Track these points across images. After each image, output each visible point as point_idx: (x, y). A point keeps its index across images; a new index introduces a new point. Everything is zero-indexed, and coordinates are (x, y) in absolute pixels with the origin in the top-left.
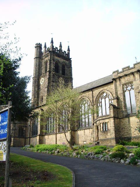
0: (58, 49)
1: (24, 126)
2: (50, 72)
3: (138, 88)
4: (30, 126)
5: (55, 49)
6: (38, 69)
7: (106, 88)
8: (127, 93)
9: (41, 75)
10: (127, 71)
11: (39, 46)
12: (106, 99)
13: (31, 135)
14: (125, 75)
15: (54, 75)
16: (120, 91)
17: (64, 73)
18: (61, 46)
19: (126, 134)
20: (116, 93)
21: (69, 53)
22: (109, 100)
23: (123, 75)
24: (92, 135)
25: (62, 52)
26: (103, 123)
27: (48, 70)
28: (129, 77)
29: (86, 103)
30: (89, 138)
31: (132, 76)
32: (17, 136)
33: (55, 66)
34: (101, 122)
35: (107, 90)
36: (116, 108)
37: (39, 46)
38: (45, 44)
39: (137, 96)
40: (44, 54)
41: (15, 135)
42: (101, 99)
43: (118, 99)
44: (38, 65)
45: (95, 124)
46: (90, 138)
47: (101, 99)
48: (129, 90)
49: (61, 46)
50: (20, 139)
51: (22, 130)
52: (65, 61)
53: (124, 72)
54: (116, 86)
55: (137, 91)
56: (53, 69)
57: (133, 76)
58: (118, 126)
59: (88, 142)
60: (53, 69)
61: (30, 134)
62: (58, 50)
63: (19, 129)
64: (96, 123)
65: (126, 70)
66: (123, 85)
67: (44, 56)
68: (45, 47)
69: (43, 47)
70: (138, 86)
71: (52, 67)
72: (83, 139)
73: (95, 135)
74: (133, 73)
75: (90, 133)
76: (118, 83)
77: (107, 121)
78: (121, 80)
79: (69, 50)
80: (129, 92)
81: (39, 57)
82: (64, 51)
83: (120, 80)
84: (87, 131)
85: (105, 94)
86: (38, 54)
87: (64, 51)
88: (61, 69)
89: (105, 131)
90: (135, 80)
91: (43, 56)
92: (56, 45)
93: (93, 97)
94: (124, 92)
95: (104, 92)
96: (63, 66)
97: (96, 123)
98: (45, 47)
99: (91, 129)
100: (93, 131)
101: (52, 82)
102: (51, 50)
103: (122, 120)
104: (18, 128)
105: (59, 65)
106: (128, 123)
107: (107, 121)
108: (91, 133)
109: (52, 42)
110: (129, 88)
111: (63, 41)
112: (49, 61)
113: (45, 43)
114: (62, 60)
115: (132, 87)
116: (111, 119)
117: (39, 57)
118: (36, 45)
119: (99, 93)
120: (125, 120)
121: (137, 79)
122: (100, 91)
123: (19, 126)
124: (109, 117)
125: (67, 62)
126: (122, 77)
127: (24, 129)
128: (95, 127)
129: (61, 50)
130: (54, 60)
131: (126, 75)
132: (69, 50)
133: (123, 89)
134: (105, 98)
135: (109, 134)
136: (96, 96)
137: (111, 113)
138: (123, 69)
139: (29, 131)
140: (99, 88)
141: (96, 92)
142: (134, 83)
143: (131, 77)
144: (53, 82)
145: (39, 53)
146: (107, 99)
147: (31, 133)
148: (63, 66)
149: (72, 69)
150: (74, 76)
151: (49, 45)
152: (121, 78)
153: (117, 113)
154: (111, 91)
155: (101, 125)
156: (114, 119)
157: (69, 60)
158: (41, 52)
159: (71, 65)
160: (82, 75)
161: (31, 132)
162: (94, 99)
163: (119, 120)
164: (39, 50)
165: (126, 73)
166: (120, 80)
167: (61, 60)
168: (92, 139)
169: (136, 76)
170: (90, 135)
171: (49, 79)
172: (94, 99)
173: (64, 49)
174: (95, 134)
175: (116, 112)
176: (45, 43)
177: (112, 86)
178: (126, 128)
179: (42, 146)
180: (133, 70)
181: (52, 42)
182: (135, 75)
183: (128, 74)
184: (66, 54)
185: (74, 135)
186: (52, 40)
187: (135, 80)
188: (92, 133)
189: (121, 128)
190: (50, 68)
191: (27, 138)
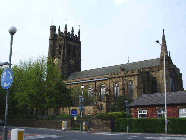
0: (71, 34)
2: (63, 55)
7: (104, 82)
8: (115, 88)
9: (55, 55)
11: (53, 29)
15: (66, 59)
16: (111, 86)
17: (74, 55)
18: (73, 31)
20: (109, 87)
21: (79, 36)
27: (62, 53)
29: (91, 89)
33: (68, 51)
34: (99, 103)
37: (53, 28)
38: (59, 28)
40: (58, 37)
42: (101, 88)
43: (110, 90)
44: (52, 46)
47: (101, 88)
49: (73, 31)
54: (109, 82)
56: (66, 53)
59: (91, 114)
60: (66, 53)
66: (113, 83)
68: (59, 30)
69: (57, 29)
71: (66, 51)
72: (88, 112)
73: (95, 110)
74: (119, 77)
76: (111, 81)
77: (102, 103)
79: (79, 33)
81: (53, 39)
84: (91, 108)
85: (103, 86)
86: (53, 36)
88: (72, 51)
89: (101, 108)
91: (57, 39)
92: (69, 30)
93: (96, 86)
94: (114, 87)
95: (102, 85)
96: (74, 49)
98: (59, 30)
101: (66, 64)
105: (71, 48)
107: (102, 103)
109: (66, 28)
110: (117, 85)
112: (63, 46)
113: (59, 26)
117: (53, 39)
125: (78, 45)
130: (67, 45)
131: (116, 77)
132: (79, 33)
133: (113, 85)
134: (103, 88)
135: (103, 111)
136: (98, 86)
141: (98, 84)
143: (118, 79)
144: (66, 64)
146: (104, 89)
148: (74, 49)
151: (63, 30)
155: (99, 105)
156: (106, 103)
160: (89, 62)
162: (97, 88)
166: (112, 80)
167: (73, 44)
171: (63, 61)
172: (97, 88)
176: (59, 26)
177: (108, 81)
179: (21, 129)
181: (66, 28)
184: (77, 38)
186: (66, 26)
188: (93, 109)
190: (64, 52)
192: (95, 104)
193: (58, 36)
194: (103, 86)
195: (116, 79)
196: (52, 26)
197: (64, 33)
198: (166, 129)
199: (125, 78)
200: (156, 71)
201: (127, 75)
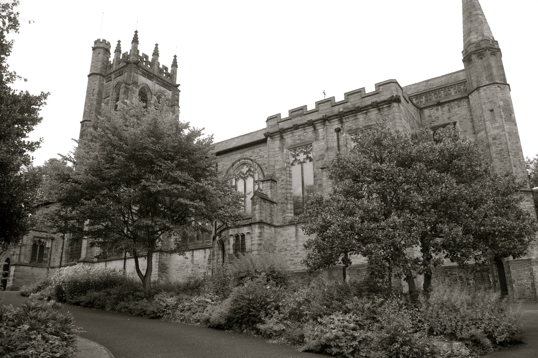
0: (150, 60)
1: (46, 239)
3: (323, 159)
4: (64, 239)
5: (141, 58)
6: (95, 103)
7: (248, 153)
10: (299, 118)
11: (101, 48)
12: (247, 181)
13: (63, 259)
14: (294, 125)
18: (156, 54)
19: (289, 262)
21: (174, 72)
22: (255, 182)
23: (291, 125)
24: (209, 263)
25: (159, 67)
26: (237, 236)
28: (303, 132)
30: (202, 271)
31: (310, 129)
32: (27, 262)
35: (252, 158)
36: (269, 201)
39: (318, 176)
41: (19, 259)
44: (96, 91)
45: (217, 238)
46: (206, 271)
48: (302, 160)
49: (156, 54)
50: (35, 269)
51: (43, 247)
52: (163, 89)
53: (294, 120)
55: (320, 164)
57: (313, 129)
58: (271, 244)
61: (61, 258)
62: (147, 62)
63: (35, 246)
64: (220, 236)
65: (297, 116)
67: (114, 72)
68: (118, 50)
69: (112, 50)
70: (322, 152)
74: (312, 123)
75: (205, 257)
77: (245, 230)
78: (285, 137)
79: (175, 64)
80: (302, 165)
82: (163, 66)
83: (282, 138)
86: (100, 67)
87: (163, 66)
90: (316, 139)
92: (145, 49)
97: (220, 236)
98: (118, 50)
99: (207, 250)
100: (213, 255)
102: (131, 59)
103: (279, 230)
104: (29, 241)
106: (294, 239)
108: (207, 256)
109: (135, 41)
111: (160, 41)
113: (119, 41)
114: (157, 86)
115: (310, 155)
116: (255, 227)
118: (96, 42)
119: (233, 165)
120: (287, 231)
121: (320, 138)
122: (234, 161)
123: (35, 237)
124: (250, 221)
125: (169, 93)
126: (287, 129)
127: (48, 245)
128: (217, 245)
129: (155, 62)
131: (296, 127)
132: (175, 64)
134: (244, 179)
137: (256, 212)
138: (291, 112)
139: (60, 250)
140: (233, 153)
142: (315, 145)
145: (103, 64)
147: (63, 256)
149: (180, 109)
150: (90, 53)
152: (285, 133)
153: (270, 214)
154: (259, 163)
157: (174, 88)
158: (108, 62)
159: (178, 101)
161: (64, 253)
163: (273, 228)
164: (101, 56)
165: (298, 121)
166: (282, 138)
168: (210, 274)
169: (319, 130)
170: (206, 265)
173: (165, 61)
174: (215, 261)
175: (269, 210)
178: (288, 249)
180: (313, 117)
181: (135, 41)
182: (317, 128)
183: (302, 125)
185: (166, 262)
187: (316, 139)
188: (209, 260)
189: (277, 249)
191: (53, 268)
192: (214, 238)
193: (115, 64)
194: (245, 169)
195: (298, 133)
196: (99, 40)
197: (129, 54)
198: (37, 258)
199: (336, 124)
200: (449, 102)
201: (347, 108)
